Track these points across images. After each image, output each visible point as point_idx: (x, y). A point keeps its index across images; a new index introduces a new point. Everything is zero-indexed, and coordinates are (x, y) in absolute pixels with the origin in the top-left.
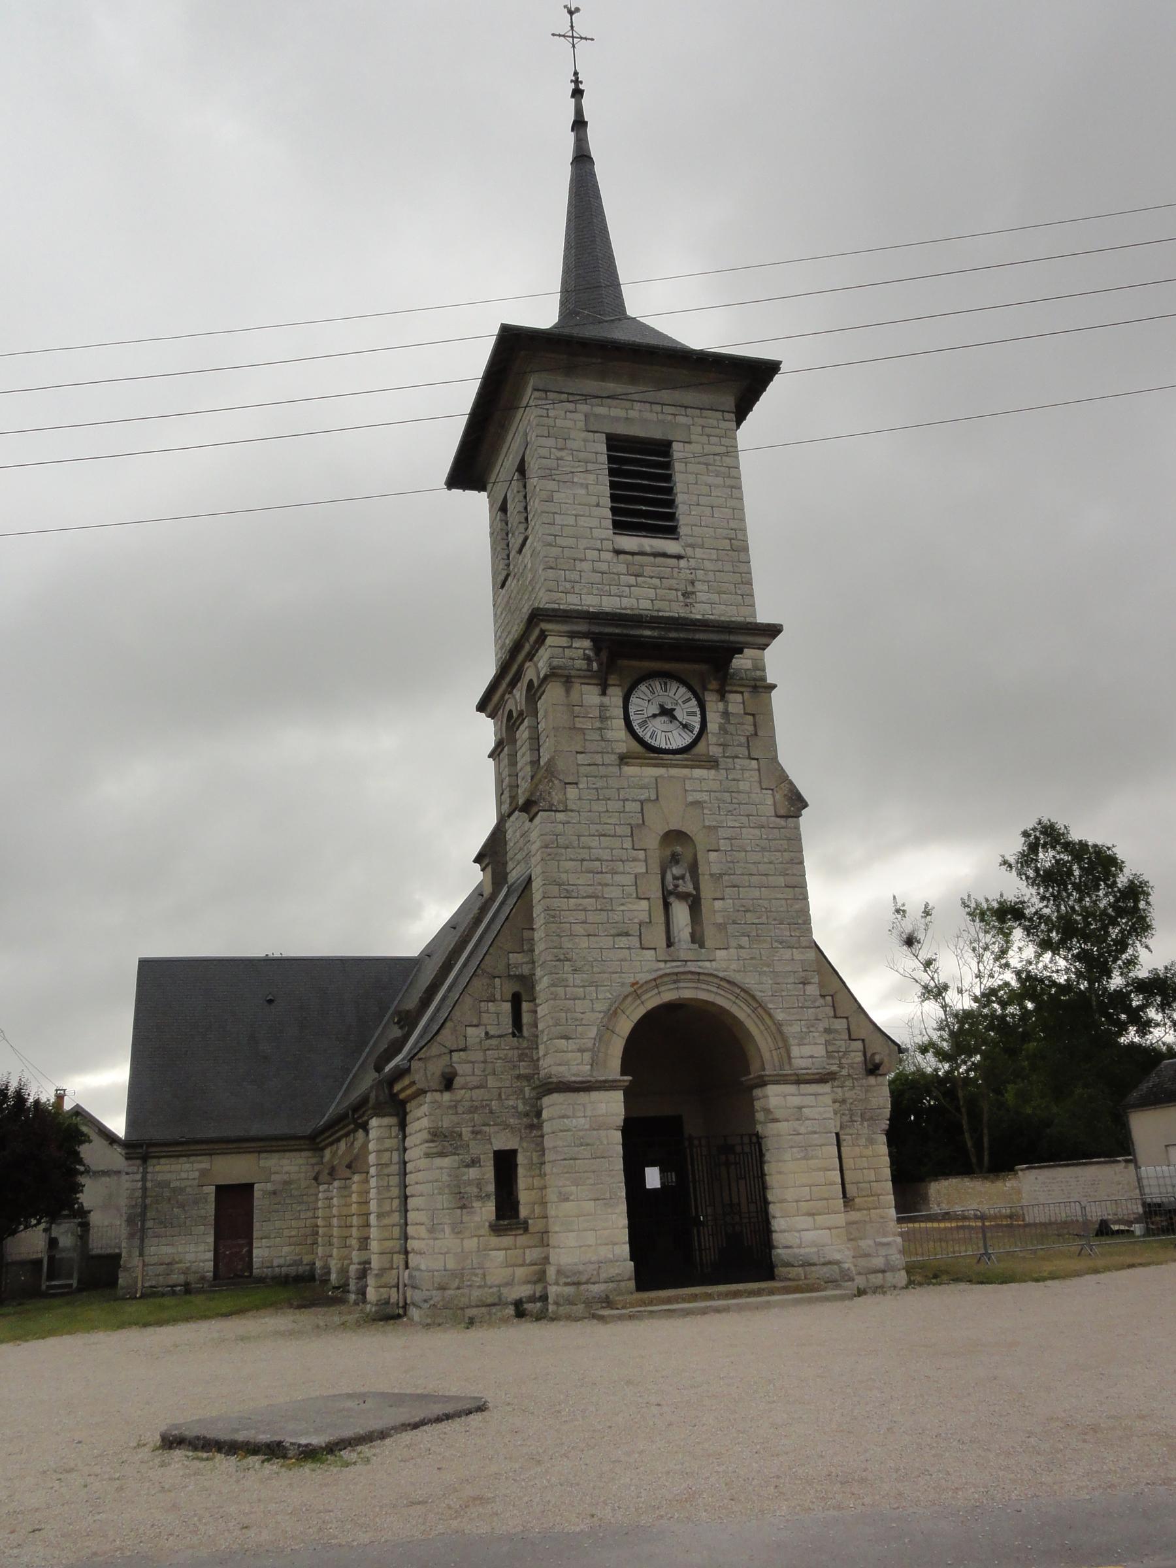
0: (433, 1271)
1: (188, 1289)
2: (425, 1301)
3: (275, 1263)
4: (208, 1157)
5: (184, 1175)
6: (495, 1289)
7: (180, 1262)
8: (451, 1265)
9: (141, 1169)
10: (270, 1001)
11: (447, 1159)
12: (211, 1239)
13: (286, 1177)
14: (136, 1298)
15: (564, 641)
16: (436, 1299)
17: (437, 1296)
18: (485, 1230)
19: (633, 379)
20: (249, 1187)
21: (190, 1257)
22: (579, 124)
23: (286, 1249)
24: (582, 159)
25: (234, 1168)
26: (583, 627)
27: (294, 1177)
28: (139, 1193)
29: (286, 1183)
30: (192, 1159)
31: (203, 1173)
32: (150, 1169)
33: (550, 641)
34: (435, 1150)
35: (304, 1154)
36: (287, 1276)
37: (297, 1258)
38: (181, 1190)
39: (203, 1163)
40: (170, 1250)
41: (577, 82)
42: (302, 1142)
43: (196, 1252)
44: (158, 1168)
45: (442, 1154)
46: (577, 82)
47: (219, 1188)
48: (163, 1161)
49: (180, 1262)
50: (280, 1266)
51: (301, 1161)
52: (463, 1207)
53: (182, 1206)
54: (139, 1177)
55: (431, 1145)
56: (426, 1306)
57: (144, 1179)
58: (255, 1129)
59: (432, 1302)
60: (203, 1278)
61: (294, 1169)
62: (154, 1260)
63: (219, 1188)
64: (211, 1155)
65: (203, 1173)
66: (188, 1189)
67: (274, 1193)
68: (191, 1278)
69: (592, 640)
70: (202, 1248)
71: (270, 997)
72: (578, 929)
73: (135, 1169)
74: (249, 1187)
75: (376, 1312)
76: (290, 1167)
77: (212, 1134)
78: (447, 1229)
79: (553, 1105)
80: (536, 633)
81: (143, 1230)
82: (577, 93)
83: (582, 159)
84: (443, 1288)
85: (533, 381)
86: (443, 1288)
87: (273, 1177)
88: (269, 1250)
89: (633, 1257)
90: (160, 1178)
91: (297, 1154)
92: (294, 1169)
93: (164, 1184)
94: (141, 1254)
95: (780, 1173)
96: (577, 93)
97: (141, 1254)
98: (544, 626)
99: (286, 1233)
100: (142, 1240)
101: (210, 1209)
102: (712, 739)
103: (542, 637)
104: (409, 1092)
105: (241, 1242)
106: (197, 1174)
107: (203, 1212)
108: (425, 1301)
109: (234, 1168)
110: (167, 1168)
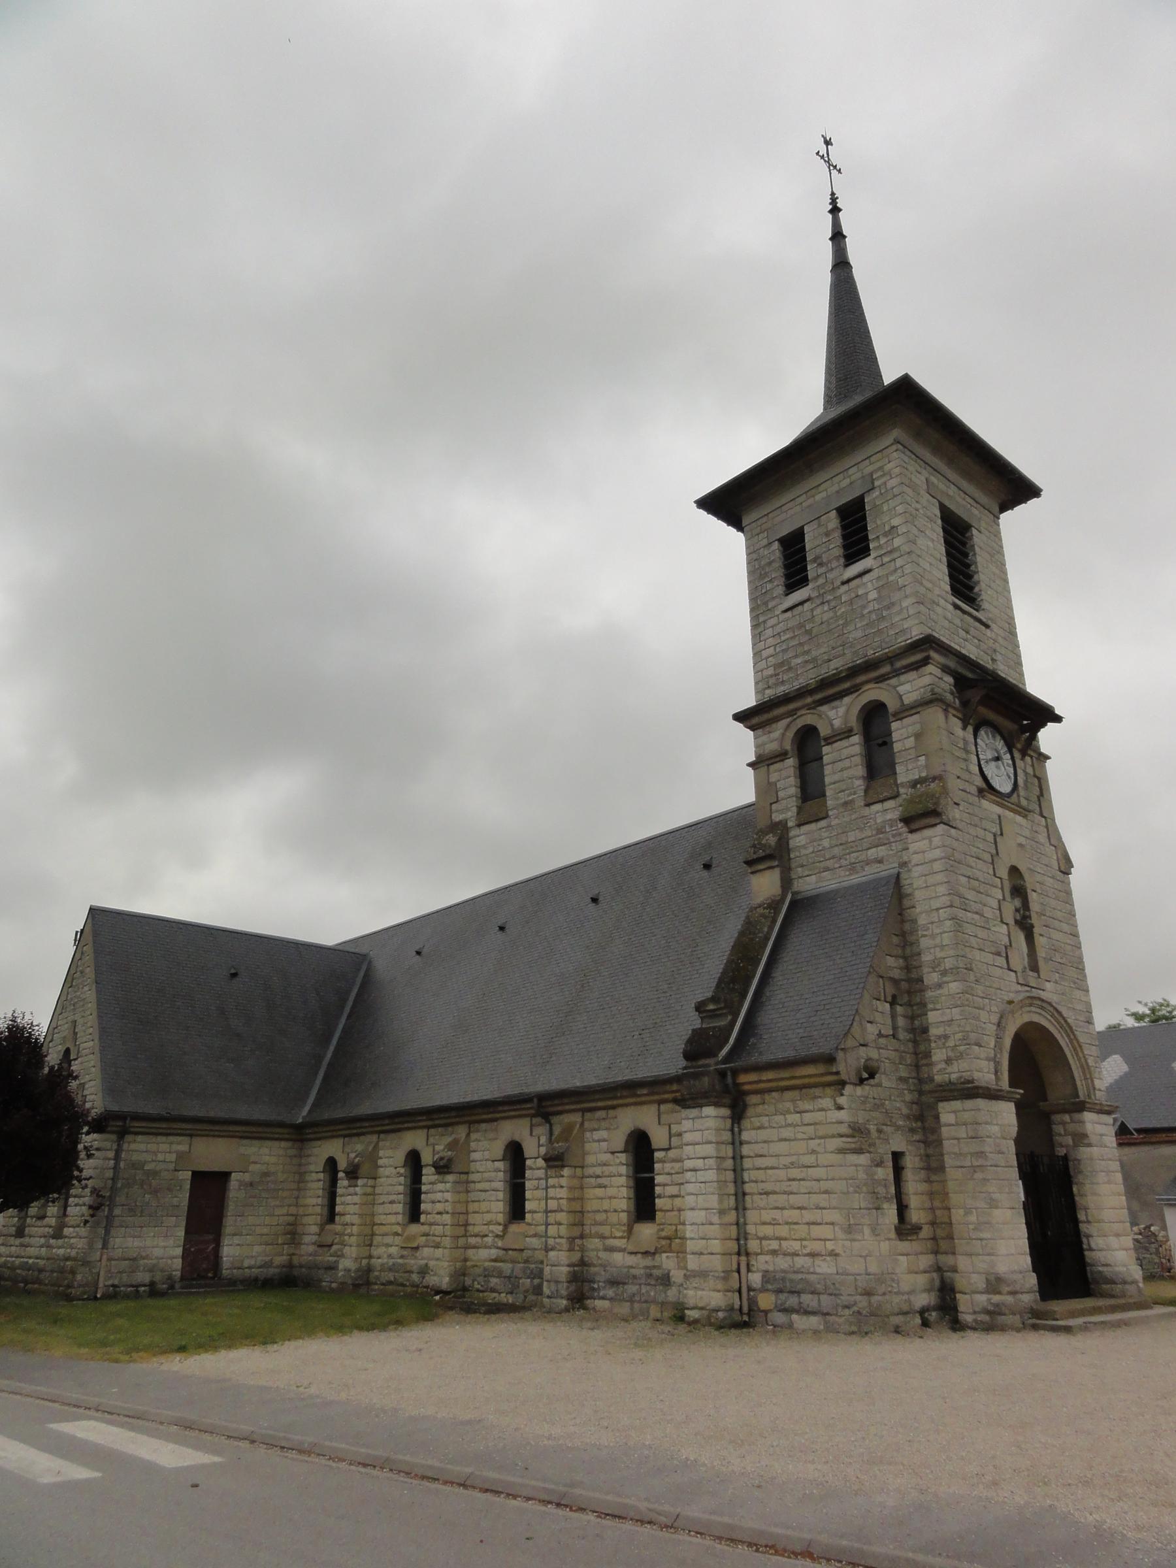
0: (137, 1286)
1: (154, 1291)
2: (847, 1307)
3: (246, 1264)
4: (187, 1139)
5: (160, 1157)
6: (905, 1297)
7: (146, 1257)
8: (873, 1268)
9: (115, 1146)
10: (234, 975)
11: (862, 1156)
12: (181, 1233)
13: (264, 1168)
14: (96, 1298)
15: (938, 672)
16: (860, 1305)
17: (862, 1302)
18: (893, 1235)
19: (950, 462)
20: (224, 1176)
21: (158, 1252)
22: (838, 236)
23: (257, 1249)
24: (841, 265)
25: (213, 1153)
26: (952, 664)
27: (272, 1169)
28: (110, 1174)
29: (266, 1174)
30: (171, 1138)
31: (181, 1156)
32: (125, 1146)
33: (930, 668)
34: (853, 1146)
35: (283, 1144)
36: (256, 1279)
37: (267, 1259)
38: (155, 1173)
39: (181, 1145)
40: (137, 1243)
41: (834, 200)
42: (286, 1131)
43: (162, 1246)
44: (133, 1146)
45: (859, 1151)
46: (834, 200)
47: (195, 1174)
48: (140, 1138)
49: (146, 1257)
50: (250, 1268)
51: (281, 1152)
52: (877, 1209)
53: (155, 1192)
54: (111, 1154)
55: (849, 1140)
56: (847, 1312)
57: (117, 1158)
58: (243, 1111)
59: (855, 1308)
60: (170, 1277)
61: (273, 1160)
62: (118, 1253)
63: (195, 1174)
64: (191, 1136)
65: (181, 1156)
66: (164, 1174)
67: (251, 1184)
68: (158, 1277)
69: (955, 678)
70: (171, 1242)
71: (233, 971)
72: (973, 941)
73: (108, 1145)
74: (224, 1176)
75: (725, 1318)
76: (267, 1156)
77: (202, 1113)
78: (867, 1231)
79: (948, 1112)
80: (919, 657)
81: (110, 1219)
82: (835, 210)
83: (841, 265)
84: (868, 1293)
85: (896, 433)
86: (868, 1293)
87: (252, 1168)
88: (242, 1247)
89: (1035, 1269)
90: (135, 1157)
91: (276, 1143)
92: (273, 1160)
93: (137, 1166)
94: (105, 1245)
95: (1095, 1194)
96: (835, 210)
97: (105, 1245)
98: (933, 654)
99: (258, 1230)
100: (107, 1232)
101: (183, 1198)
102: (1022, 792)
103: (925, 662)
104: (754, 1087)
105: (211, 1237)
106: (173, 1157)
107: (175, 1201)
108: (847, 1307)
109: (213, 1153)
110: (142, 1147)
